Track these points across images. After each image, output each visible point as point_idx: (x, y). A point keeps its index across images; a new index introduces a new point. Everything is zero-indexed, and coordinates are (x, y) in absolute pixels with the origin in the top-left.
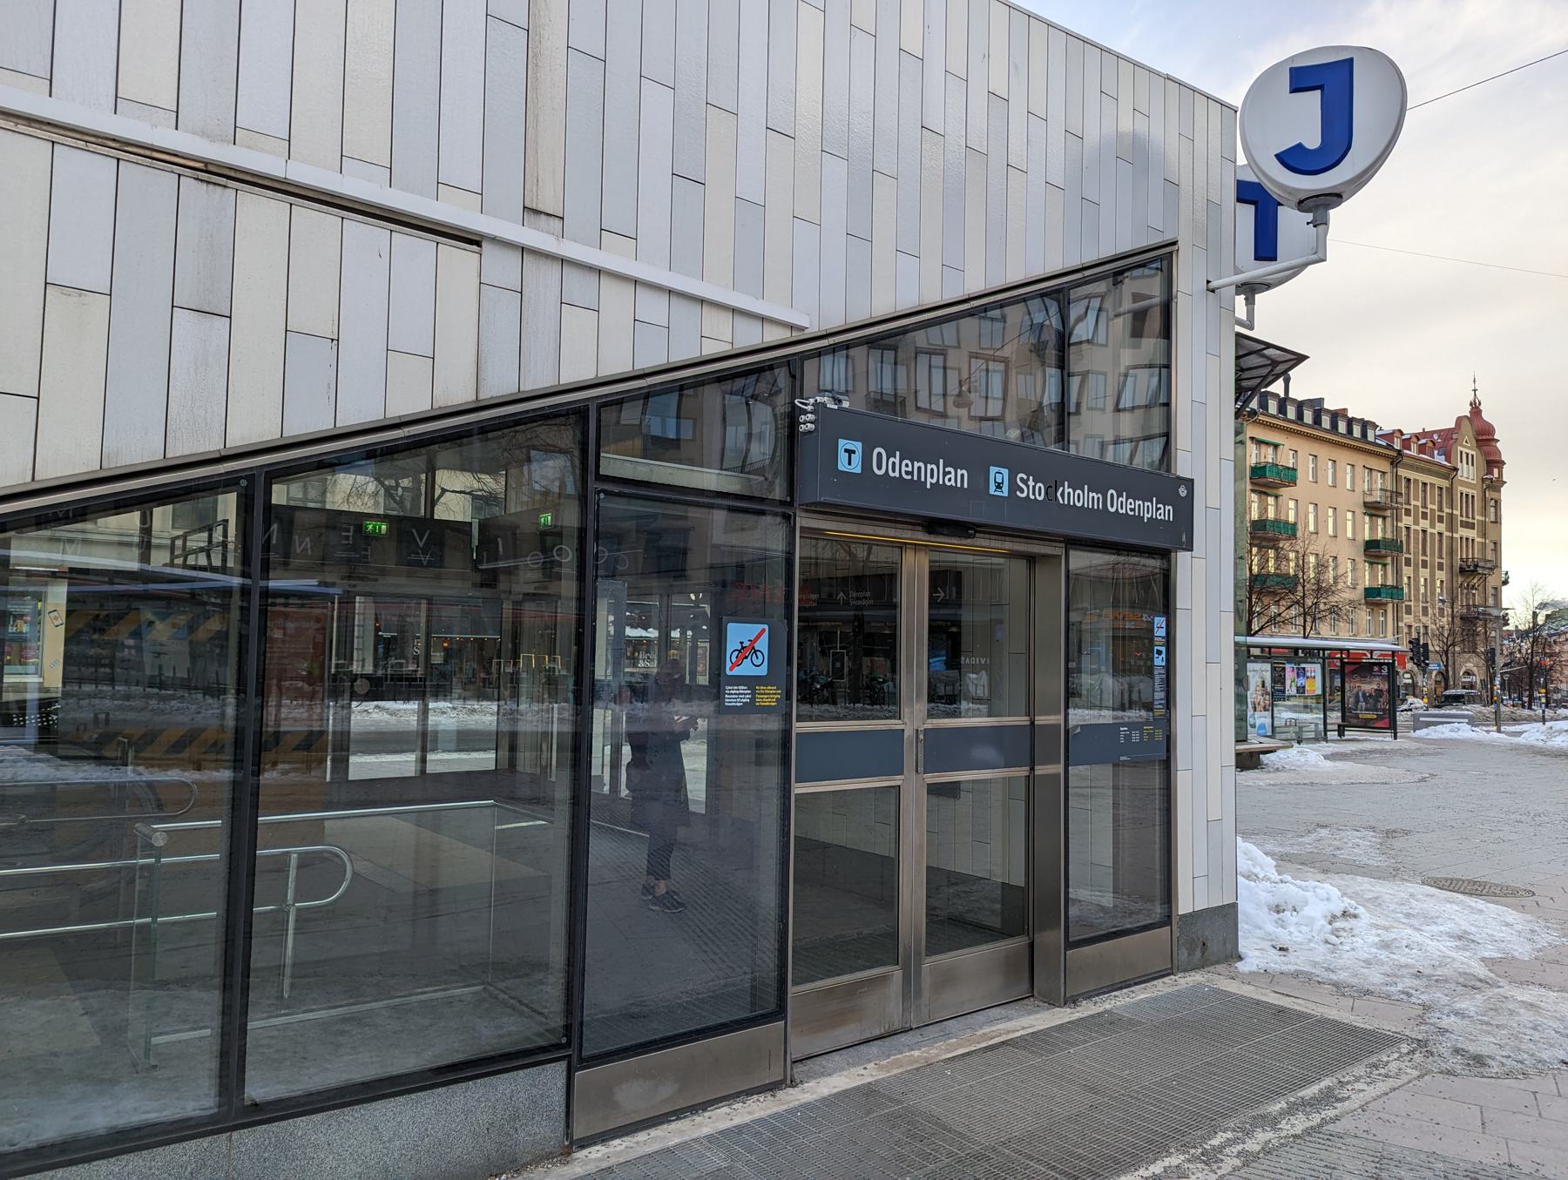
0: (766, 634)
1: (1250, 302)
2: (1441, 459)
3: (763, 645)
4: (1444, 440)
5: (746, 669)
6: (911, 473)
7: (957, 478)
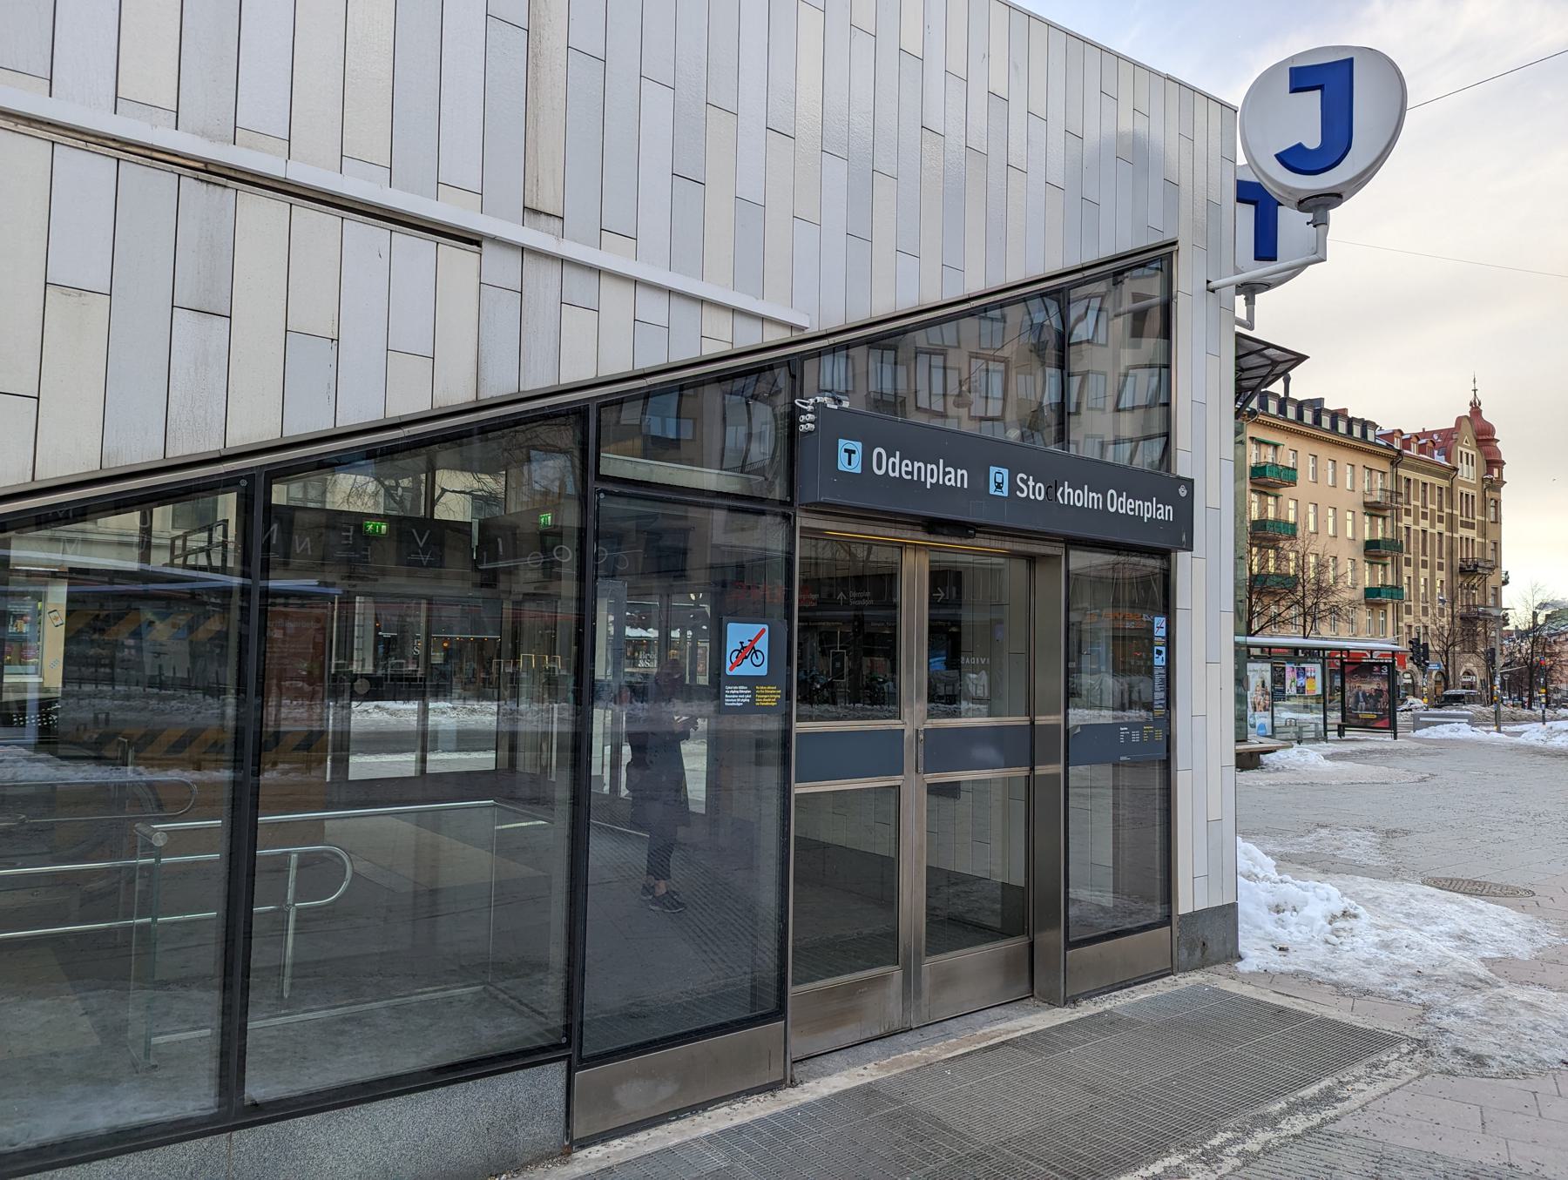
0: (766, 634)
1: (1250, 302)
2: (1441, 459)
3: (763, 645)
4: (1444, 440)
5: (746, 669)
6: (911, 473)
7: (957, 478)
